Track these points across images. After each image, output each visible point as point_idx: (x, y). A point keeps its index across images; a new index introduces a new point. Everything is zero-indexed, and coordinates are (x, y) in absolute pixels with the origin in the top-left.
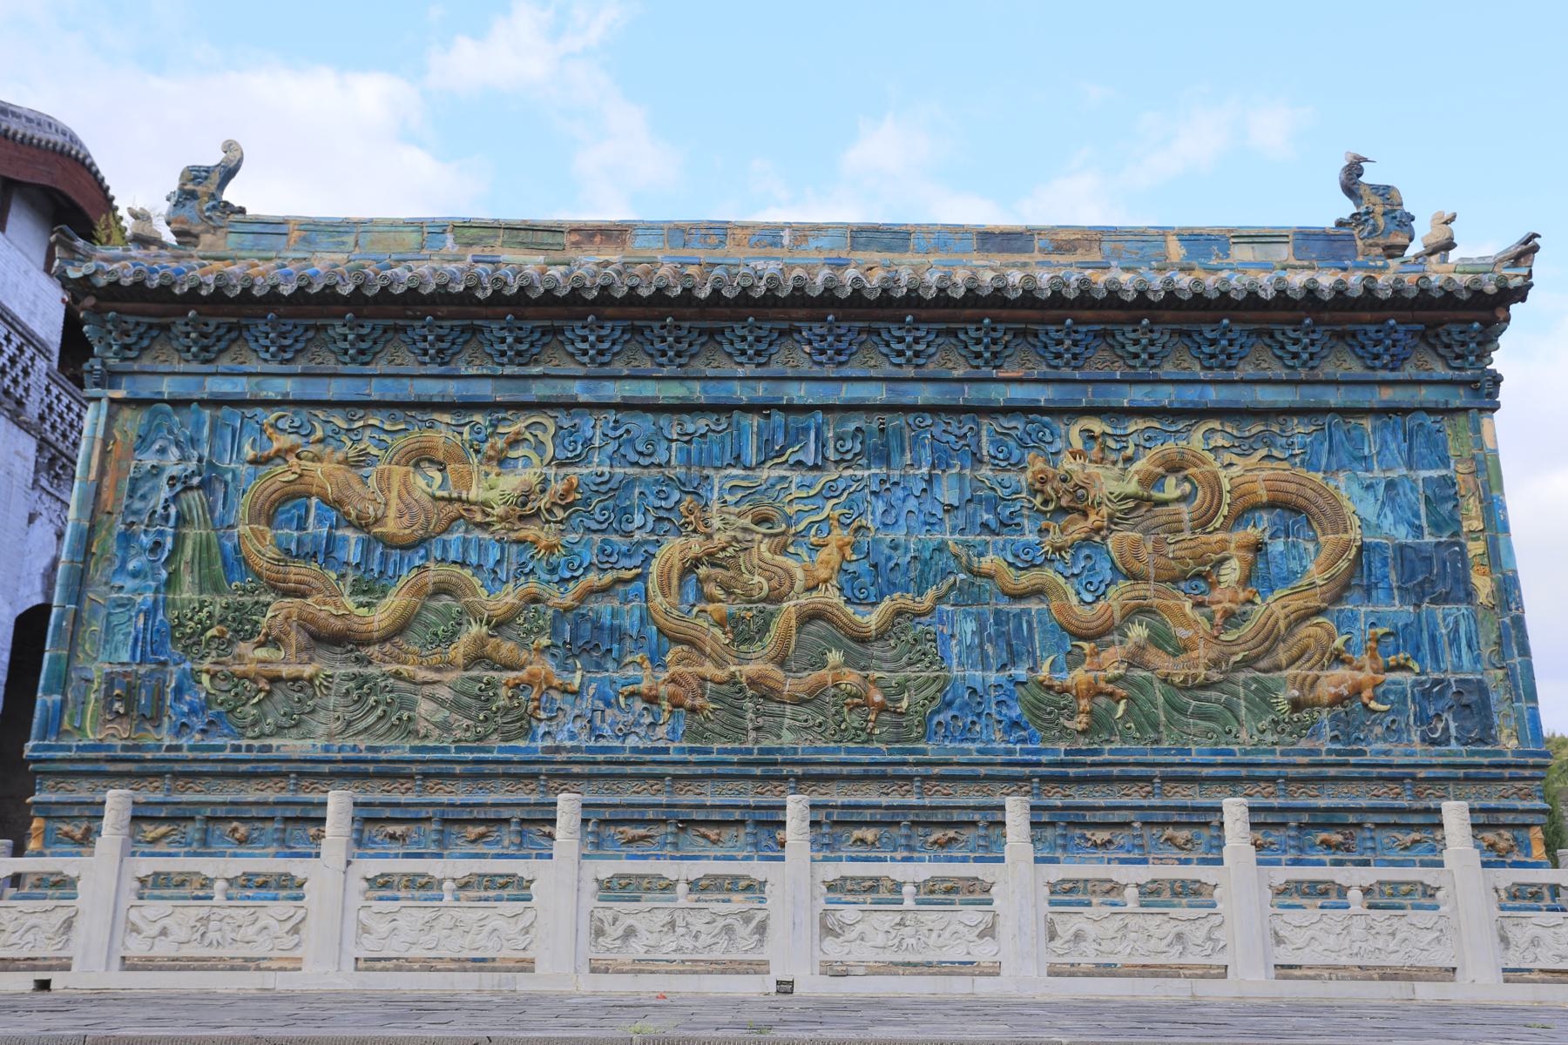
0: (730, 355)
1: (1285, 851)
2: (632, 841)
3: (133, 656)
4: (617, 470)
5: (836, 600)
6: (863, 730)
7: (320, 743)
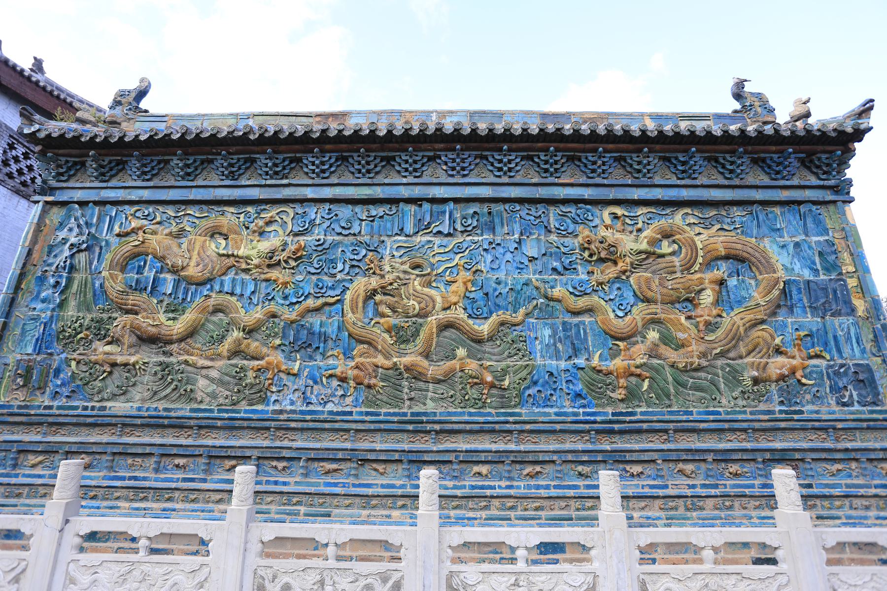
0: (399, 172)
1: (755, 478)
2: (328, 472)
3: (34, 350)
4: (329, 238)
5: (462, 316)
6: (479, 400)
7: (136, 405)
